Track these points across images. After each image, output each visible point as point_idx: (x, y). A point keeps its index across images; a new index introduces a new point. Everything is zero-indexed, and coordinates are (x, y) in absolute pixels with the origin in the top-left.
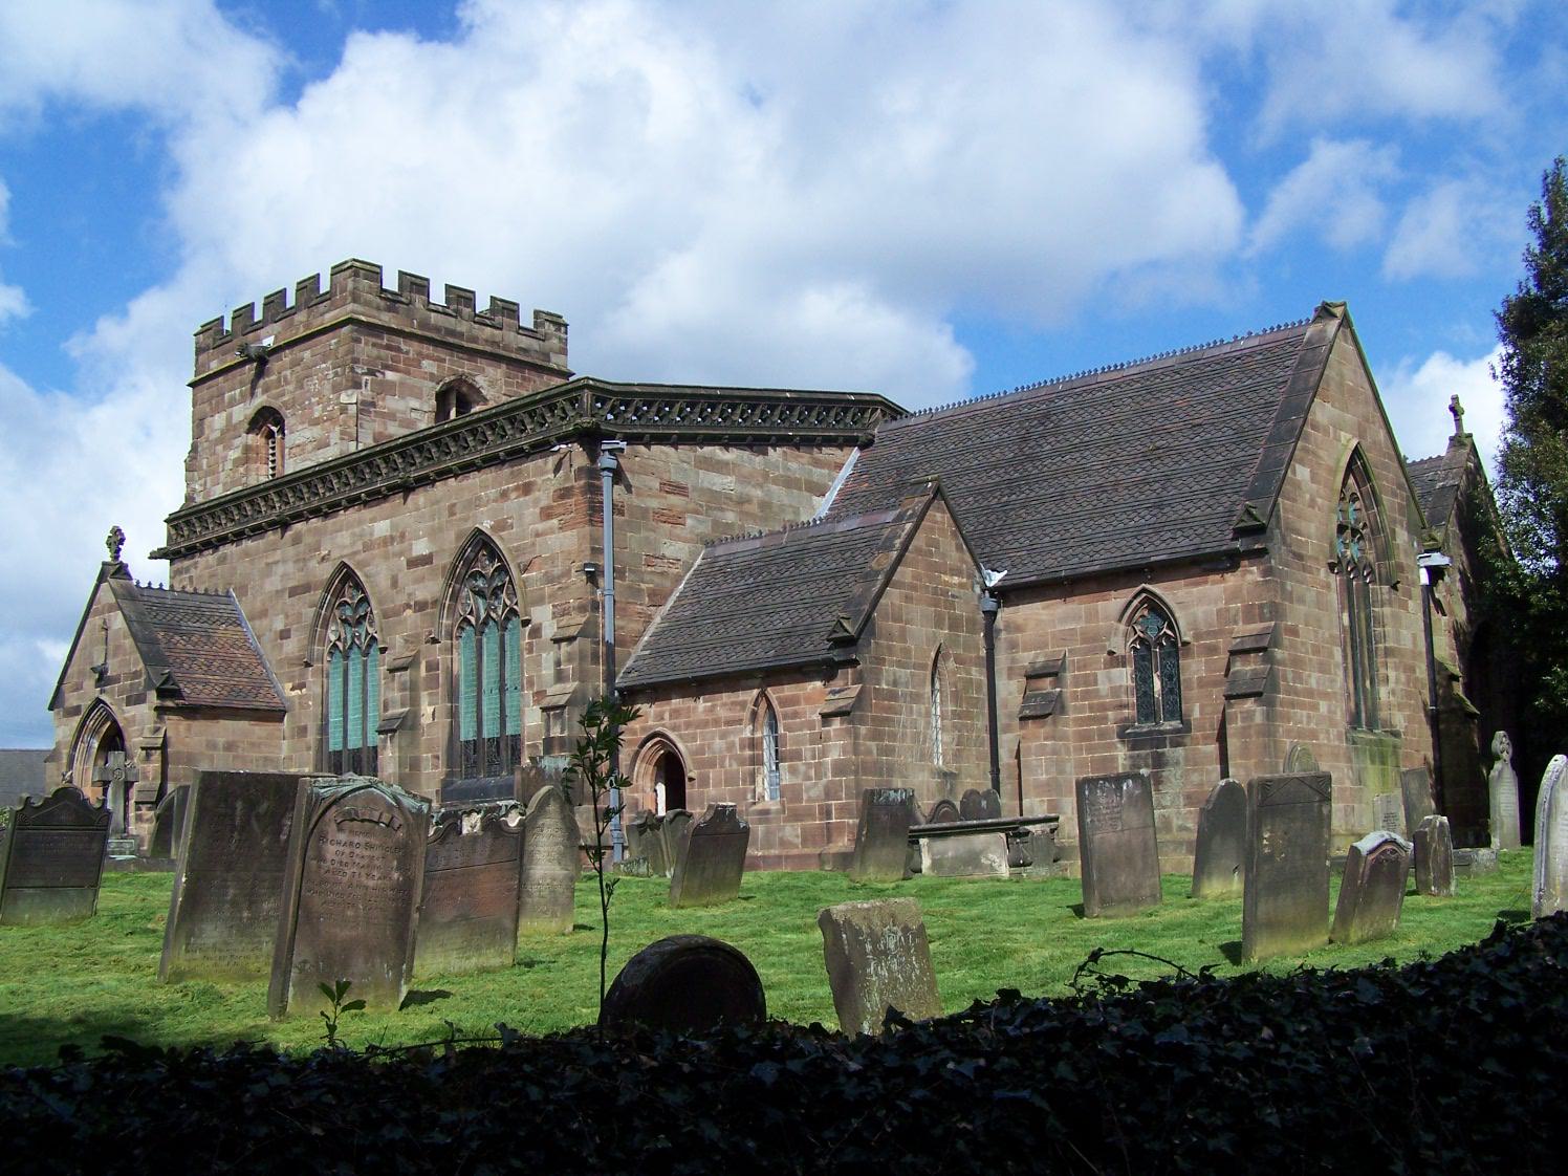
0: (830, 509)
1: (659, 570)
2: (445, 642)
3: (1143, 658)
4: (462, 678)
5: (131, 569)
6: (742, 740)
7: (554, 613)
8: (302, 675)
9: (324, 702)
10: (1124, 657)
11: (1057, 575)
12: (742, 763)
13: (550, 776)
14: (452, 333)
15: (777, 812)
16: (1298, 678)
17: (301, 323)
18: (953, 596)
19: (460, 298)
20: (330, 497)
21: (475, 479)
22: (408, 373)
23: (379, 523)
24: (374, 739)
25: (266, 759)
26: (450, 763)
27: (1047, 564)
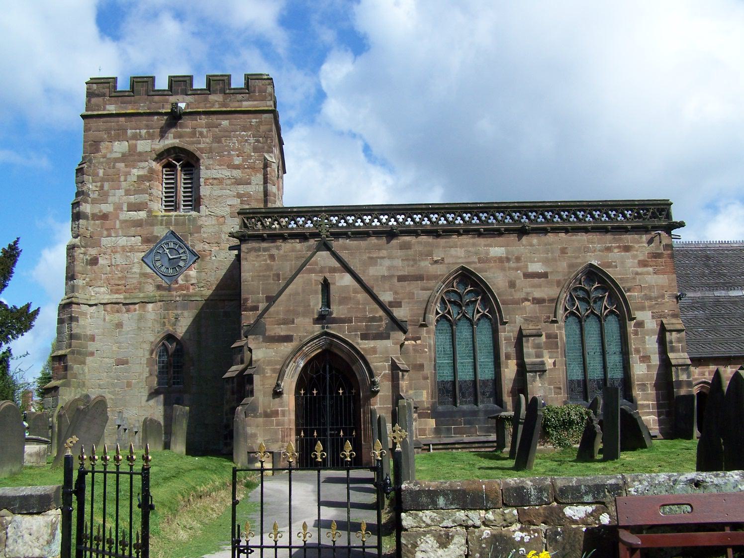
7: (652, 316)
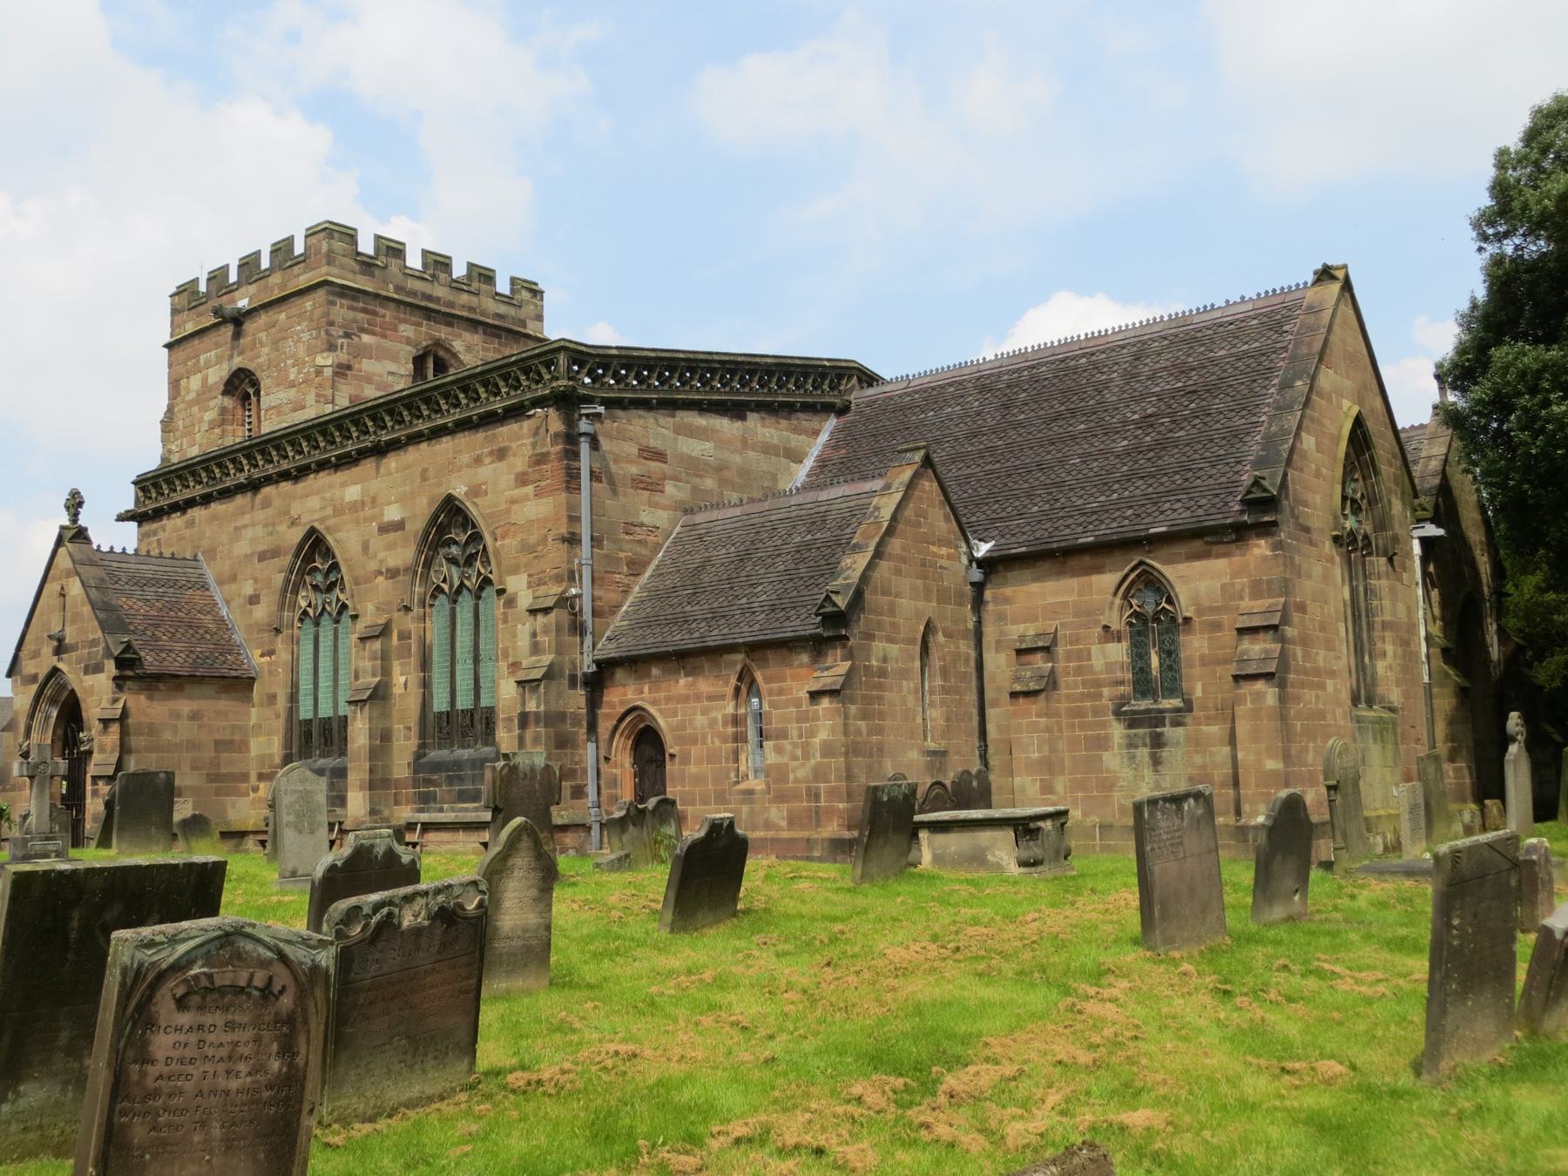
0: (808, 476)
1: (639, 537)
2: (417, 610)
3: (1139, 633)
4: (435, 648)
5: (91, 533)
6: (724, 717)
7: (529, 583)
8: (272, 642)
9: (294, 668)
10: (1119, 632)
11: (1049, 546)
12: (724, 741)
13: (525, 774)
14: (429, 298)
15: (763, 792)
16: (1307, 656)
17: (276, 286)
18: (941, 567)
19: (438, 264)
20: (300, 461)
21: (446, 444)
22: (384, 336)
23: (349, 487)
24: (344, 709)
25: (233, 727)
26: (423, 735)
27: (1038, 535)
